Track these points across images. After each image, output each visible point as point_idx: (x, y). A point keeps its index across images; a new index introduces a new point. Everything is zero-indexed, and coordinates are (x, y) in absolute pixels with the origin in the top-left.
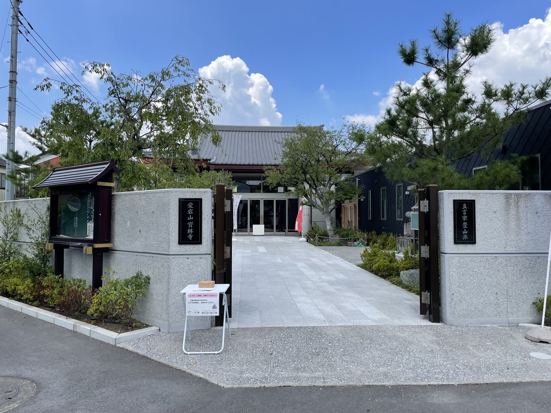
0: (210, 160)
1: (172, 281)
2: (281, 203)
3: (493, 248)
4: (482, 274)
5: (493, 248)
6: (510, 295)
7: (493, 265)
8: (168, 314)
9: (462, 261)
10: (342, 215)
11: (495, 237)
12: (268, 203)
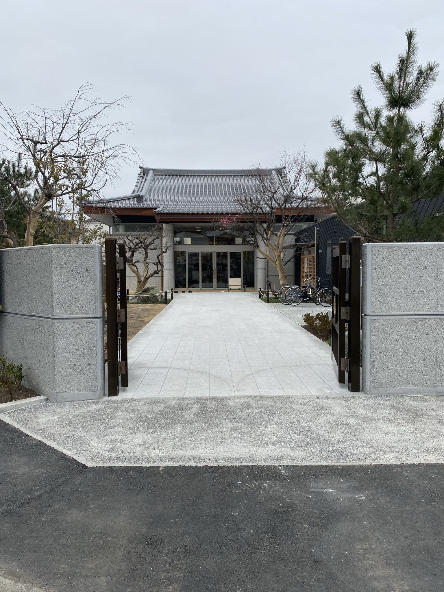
0: (156, 209)
1: (57, 347)
2: (235, 256)
3: (422, 309)
4: (408, 338)
5: (422, 309)
6: (440, 361)
7: (421, 328)
8: (55, 382)
9: (385, 323)
10: (301, 269)
11: (424, 296)
12: (222, 256)
